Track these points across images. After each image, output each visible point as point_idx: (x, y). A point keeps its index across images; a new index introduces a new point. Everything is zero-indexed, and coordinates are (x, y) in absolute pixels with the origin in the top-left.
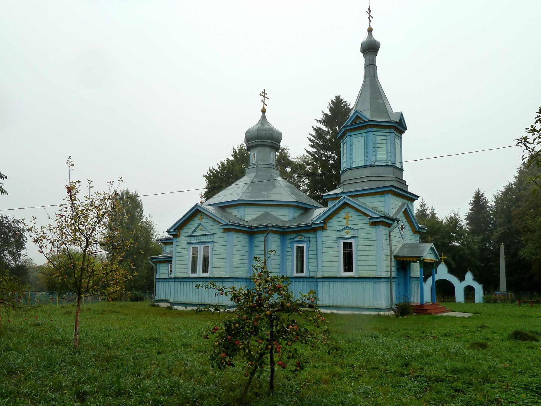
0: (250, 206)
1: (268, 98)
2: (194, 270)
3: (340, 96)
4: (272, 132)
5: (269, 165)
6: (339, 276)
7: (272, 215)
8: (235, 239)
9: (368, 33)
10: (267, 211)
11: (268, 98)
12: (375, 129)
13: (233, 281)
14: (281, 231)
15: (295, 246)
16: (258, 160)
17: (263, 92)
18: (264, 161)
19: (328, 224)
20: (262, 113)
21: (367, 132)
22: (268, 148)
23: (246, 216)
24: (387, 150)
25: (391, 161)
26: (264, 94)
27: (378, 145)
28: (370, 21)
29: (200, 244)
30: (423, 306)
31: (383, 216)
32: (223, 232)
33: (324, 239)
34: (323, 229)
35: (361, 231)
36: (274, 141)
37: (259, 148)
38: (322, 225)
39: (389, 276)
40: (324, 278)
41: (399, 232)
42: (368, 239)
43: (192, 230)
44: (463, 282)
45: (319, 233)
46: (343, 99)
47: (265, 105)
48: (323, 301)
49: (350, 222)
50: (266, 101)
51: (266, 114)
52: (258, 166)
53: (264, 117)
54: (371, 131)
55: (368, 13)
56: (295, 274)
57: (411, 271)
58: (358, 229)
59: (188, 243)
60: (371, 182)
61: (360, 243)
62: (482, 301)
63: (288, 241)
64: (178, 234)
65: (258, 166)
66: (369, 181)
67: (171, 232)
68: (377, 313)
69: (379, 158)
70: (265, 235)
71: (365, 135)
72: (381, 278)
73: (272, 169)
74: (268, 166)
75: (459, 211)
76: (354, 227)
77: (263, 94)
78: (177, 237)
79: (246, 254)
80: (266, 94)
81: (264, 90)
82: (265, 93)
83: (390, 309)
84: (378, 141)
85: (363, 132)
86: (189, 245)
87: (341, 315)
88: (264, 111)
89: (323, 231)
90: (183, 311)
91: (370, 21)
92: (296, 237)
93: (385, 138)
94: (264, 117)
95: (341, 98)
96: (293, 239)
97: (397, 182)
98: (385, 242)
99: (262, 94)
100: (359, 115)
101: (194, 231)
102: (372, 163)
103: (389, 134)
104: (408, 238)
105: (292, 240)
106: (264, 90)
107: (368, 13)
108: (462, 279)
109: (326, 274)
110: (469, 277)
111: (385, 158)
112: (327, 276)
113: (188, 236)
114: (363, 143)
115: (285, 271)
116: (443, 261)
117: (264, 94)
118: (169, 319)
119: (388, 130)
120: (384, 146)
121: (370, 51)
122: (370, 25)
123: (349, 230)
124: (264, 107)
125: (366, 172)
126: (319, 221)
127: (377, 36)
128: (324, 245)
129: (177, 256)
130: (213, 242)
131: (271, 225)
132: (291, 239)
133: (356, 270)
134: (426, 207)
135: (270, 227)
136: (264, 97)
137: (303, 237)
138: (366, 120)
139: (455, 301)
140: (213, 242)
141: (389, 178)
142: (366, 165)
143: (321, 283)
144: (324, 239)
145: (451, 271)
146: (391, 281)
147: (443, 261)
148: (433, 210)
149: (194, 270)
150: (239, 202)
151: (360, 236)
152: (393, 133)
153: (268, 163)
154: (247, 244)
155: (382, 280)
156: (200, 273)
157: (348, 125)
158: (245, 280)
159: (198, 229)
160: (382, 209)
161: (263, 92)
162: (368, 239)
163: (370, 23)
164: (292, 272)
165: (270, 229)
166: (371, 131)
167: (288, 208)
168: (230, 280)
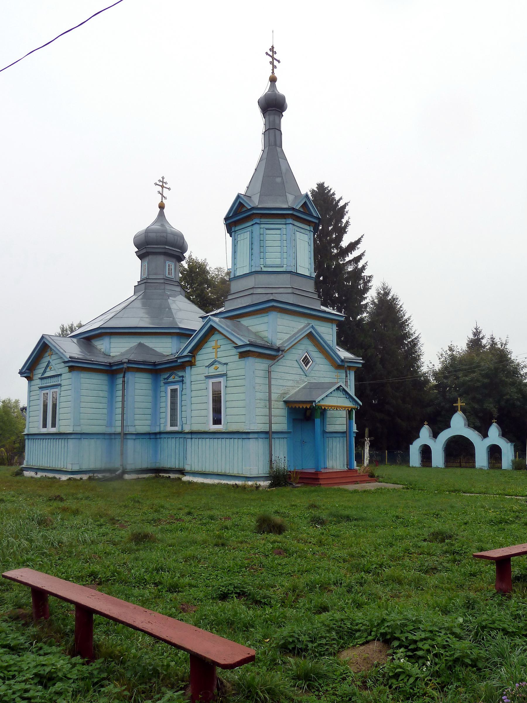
0: (125, 336)
1: (169, 189)
2: (45, 426)
3: (323, 183)
4: (165, 235)
5: (163, 280)
6: (207, 430)
7: (148, 347)
8: (83, 380)
9: (270, 83)
10: (141, 342)
11: (169, 189)
12: (263, 220)
13: (80, 437)
14: (151, 369)
15: (170, 388)
16: (148, 275)
17: (160, 181)
18: (156, 274)
19: (198, 358)
20: (159, 209)
21: (252, 225)
22: (163, 256)
23: (112, 350)
24: (281, 249)
25: (288, 265)
26: (162, 184)
27: (268, 243)
28: (274, 67)
29: (49, 388)
30: (318, 474)
31: (248, 343)
32: (69, 372)
33: (194, 378)
34: (191, 364)
35: (230, 366)
36: (169, 246)
37: (150, 257)
38: (187, 359)
39: (267, 429)
40: (192, 433)
41: (299, 367)
42: (238, 378)
43: (42, 371)
44: (486, 440)
45: (188, 369)
46: (328, 187)
47: (163, 198)
48: (191, 465)
49: (220, 354)
50: (166, 192)
51: (165, 211)
52: (149, 281)
53: (161, 214)
54: (256, 223)
55: (269, 55)
56: (169, 429)
57: (327, 423)
58: (226, 364)
59: (40, 388)
60: (254, 296)
61: (230, 383)
62: (510, 468)
63: (162, 384)
64: (31, 377)
65: (149, 281)
66: (251, 295)
67: (25, 373)
68: (254, 483)
69: (269, 262)
70: (122, 375)
71: (249, 229)
72: (248, 433)
73: (166, 285)
74: (162, 281)
75: (508, 338)
76: (223, 360)
77: (161, 184)
78: (31, 381)
79: (105, 400)
80: (166, 183)
81: (163, 178)
82: (164, 181)
83: (266, 478)
84: (268, 237)
85: (248, 225)
86: (41, 390)
87: (196, 483)
88: (162, 207)
89: (192, 367)
90: (32, 477)
91: (274, 67)
92: (169, 377)
93: (278, 232)
94: (161, 214)
95: (326, 185)
96: (167, 378)
97: (292, 295)
98: (260, 381)
99: (158, 183)
100: (242, 201)
101: (45, 372)
102: (259, 269)
103: (284, 226)
104: (322, 376)
105: (166, 381)
106: (163, 178)
107: (269, 55)
108: (485, 435)
109: (195, 428)
110: (494, 431)
111: (278, 262)
112: (195, 430)
113: (40, 379)
114: (247, 242)
115: (158, 424)
116: (459, 409)
117: (162, 184)
118: (363, 489)
119: (283, 221)
120: (278, 243)
121: (276, 109)
122: (273, 72)
123: (218, 366)
124: (162, 202)
125: (250, 282)
126: (185, 353)
127: (281, 88)
128: (194, 387)
129: (31, 405)
130: (60, 385)
131: (127, 361)
132: (165, 379)
133: (224, 422)
134: (481, 336)
135: (125, 363)
136: (162, 187)
137: (176, 377)
138: (249, 208)
139: (474, 467)
140: (60, 385)
141: (282, 289)
142: (251, 272)
143: (189, 439)
144: (194, 378)
145: (471, 424)
146: (271, 438)
147: (459, 409)
148: (492, 339)
149: (45, 426)
150: (100, 331)
151: (229, 374)
152: (291, 225)
153: (161, 277)
154: (105, 388)
155: (251, 436)
156: (50, 429)
157: (230, 216)
158: (148, 437)
159: (48, 369)
160: (265, 334)
161: (160, 181)
162: (238, 378)
163: (273, 70)
164: (165, 426)
165: (125, 366)
166: (256, 223)
167: (170, 336)
168: (73, 436)
